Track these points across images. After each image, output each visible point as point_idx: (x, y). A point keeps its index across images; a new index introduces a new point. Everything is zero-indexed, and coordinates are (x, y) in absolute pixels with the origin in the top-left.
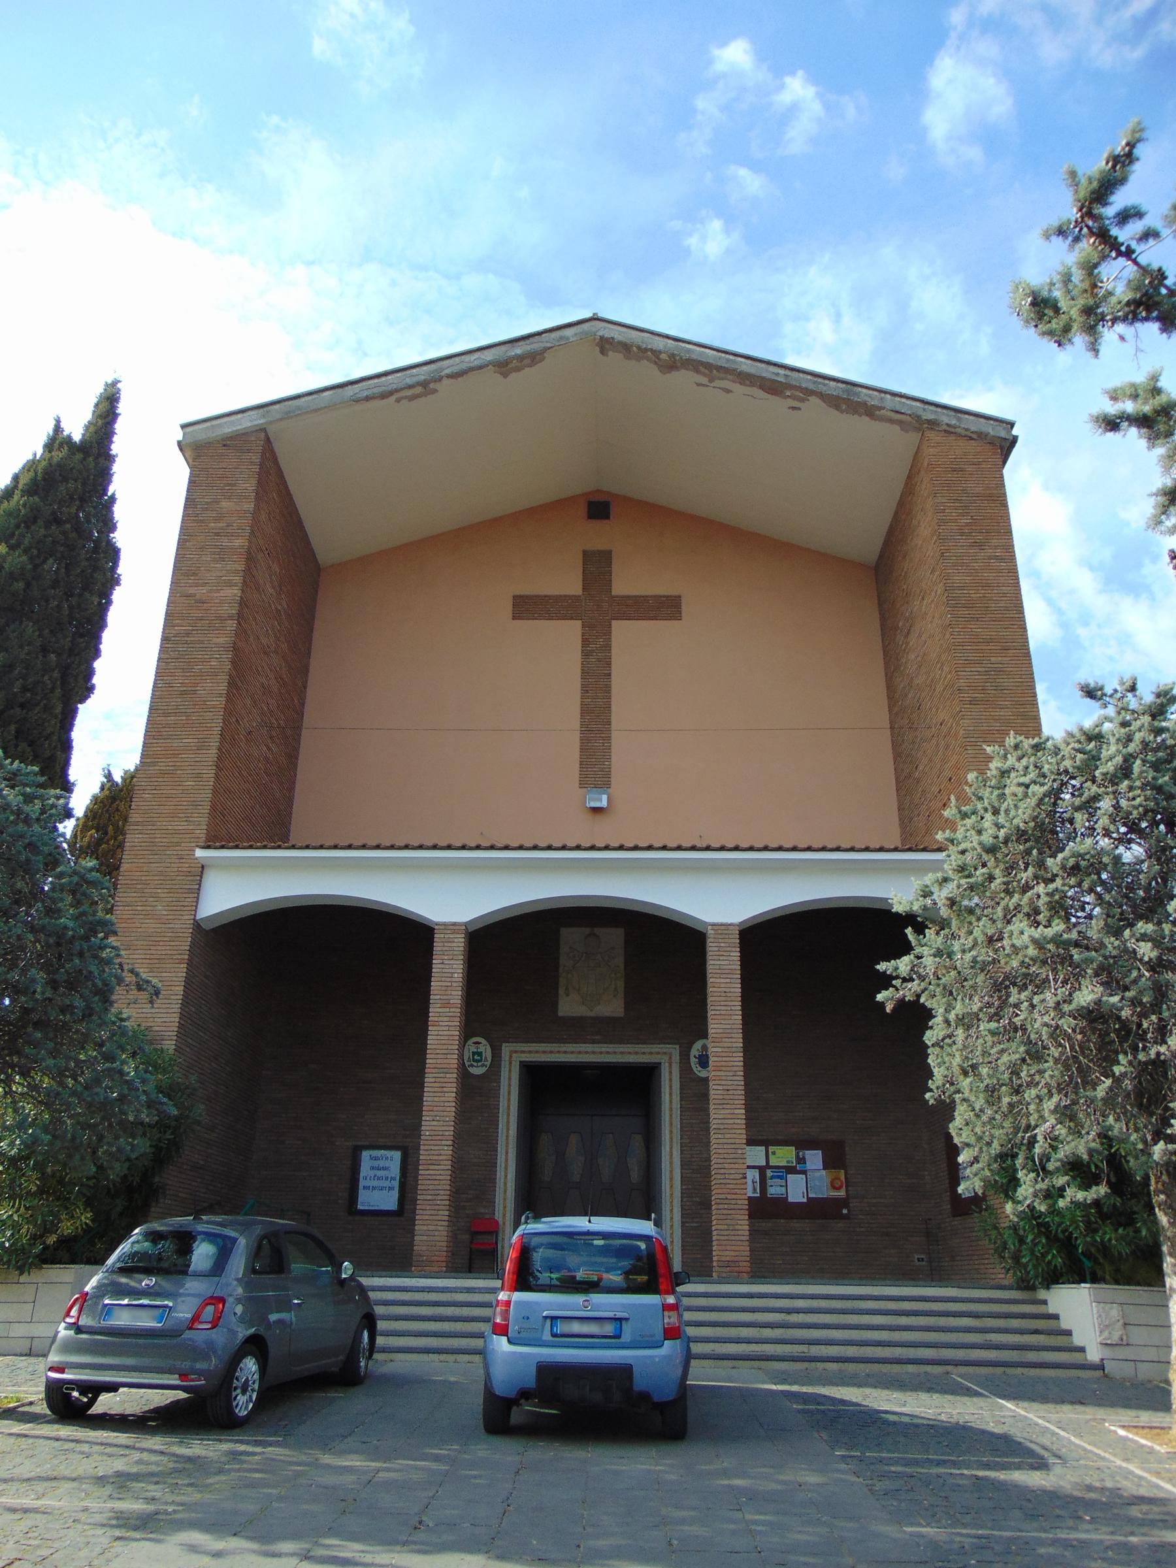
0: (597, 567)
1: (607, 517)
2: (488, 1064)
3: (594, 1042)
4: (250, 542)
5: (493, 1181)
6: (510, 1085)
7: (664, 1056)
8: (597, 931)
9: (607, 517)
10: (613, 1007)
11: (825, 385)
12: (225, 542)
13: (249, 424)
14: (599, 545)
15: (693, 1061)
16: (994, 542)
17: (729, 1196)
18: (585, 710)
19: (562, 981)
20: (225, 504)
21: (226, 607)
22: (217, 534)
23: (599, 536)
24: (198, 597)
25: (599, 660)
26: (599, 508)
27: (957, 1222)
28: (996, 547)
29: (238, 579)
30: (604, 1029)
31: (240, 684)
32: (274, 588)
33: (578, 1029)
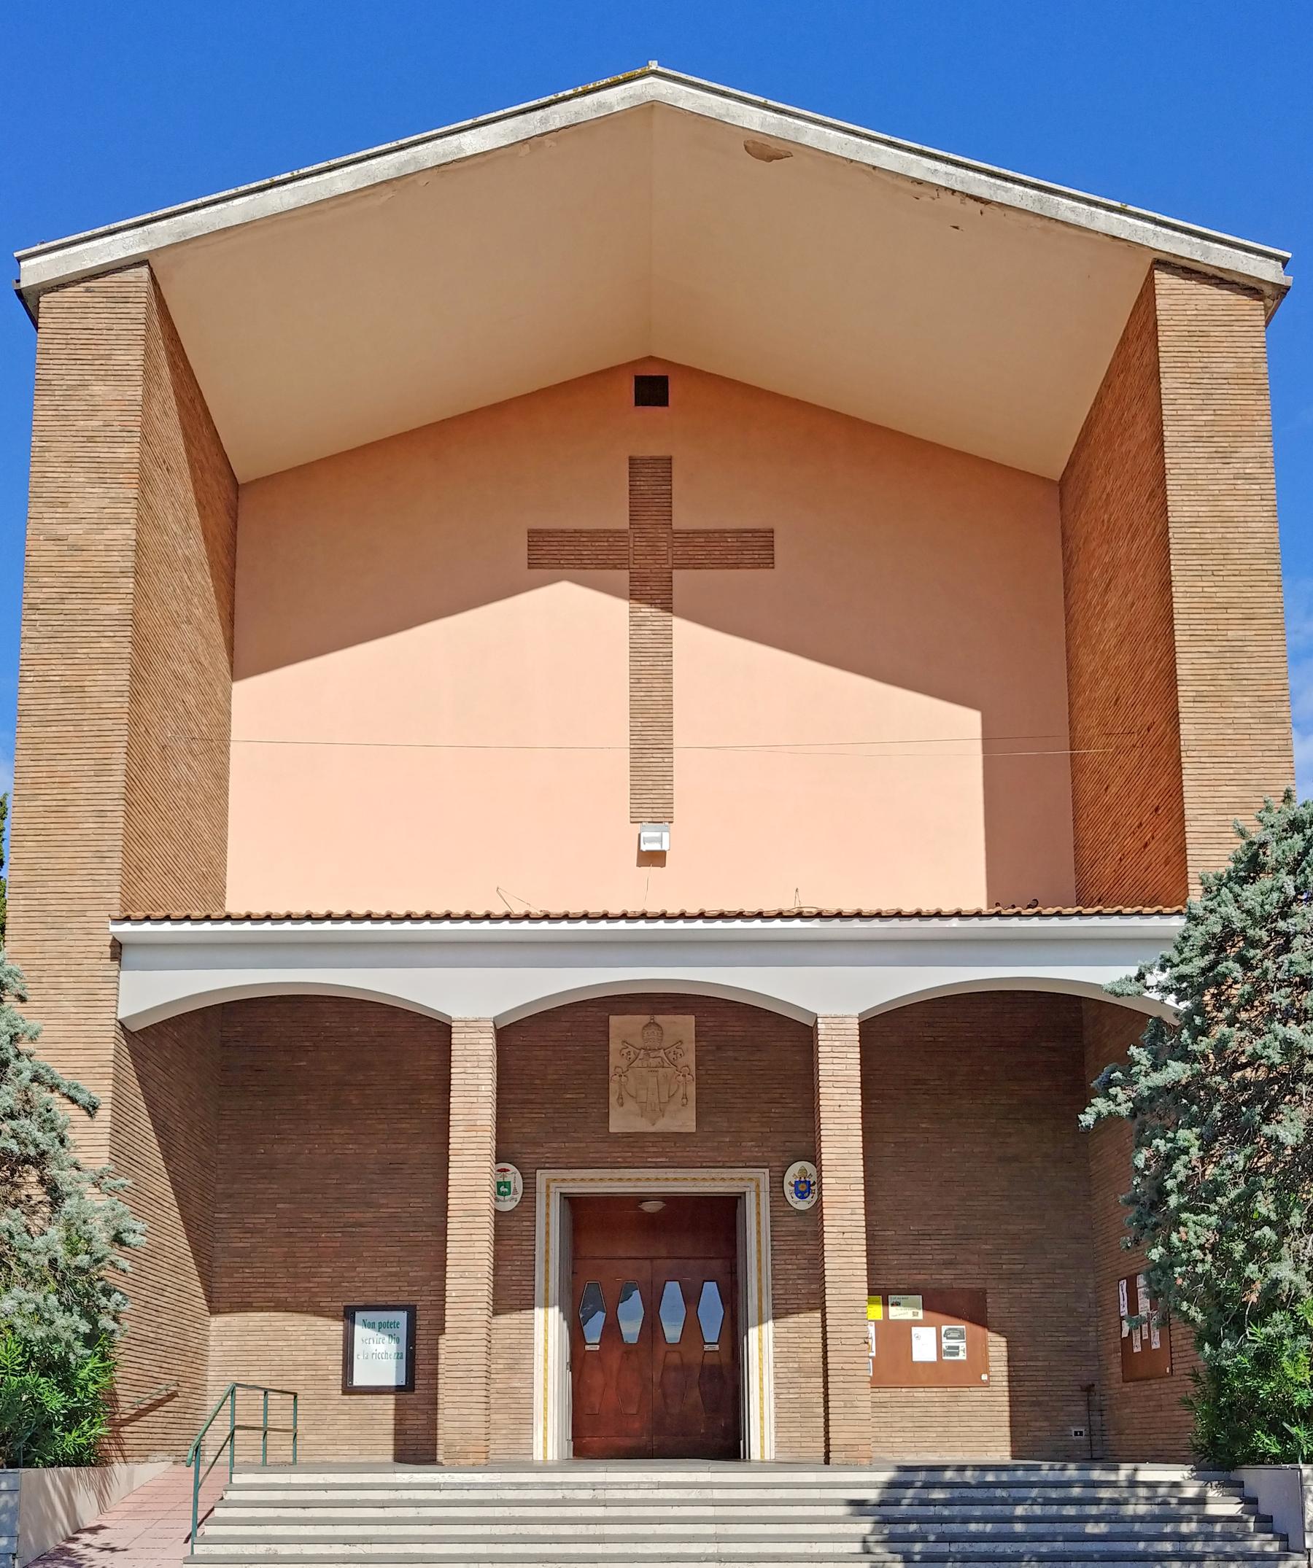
0: (652, 478)
1: (663, 401)
2: (519, 1197)
3: (657, 1166)
4: (141, 453)
5: (531, 1346)
6: (761, 1389)
7: (751, 1185)
8: (659, 1018)
9: (663, 401)
10: (685, 1121)
11: (1007, 190)
12: (102, 451)
13: (123, 256)
14: (653, 449)
15: (788, 1190)
16: (1245, 452)
17: (846, 1366)
18: (637, 711)
19: (613, 1087)
20: (98, 389)
21: (115, 556)
22: (91, 439)
23: (652, 432)
24: (71, 540)
25: (654, 633)
26: (652, 390)
27: (1129, 1388)
28: (1246, 460)
29: (129, 512)
30: (668, 1149)
31: (144, 674)
32: (180, 522)
33: (637, 1149)
